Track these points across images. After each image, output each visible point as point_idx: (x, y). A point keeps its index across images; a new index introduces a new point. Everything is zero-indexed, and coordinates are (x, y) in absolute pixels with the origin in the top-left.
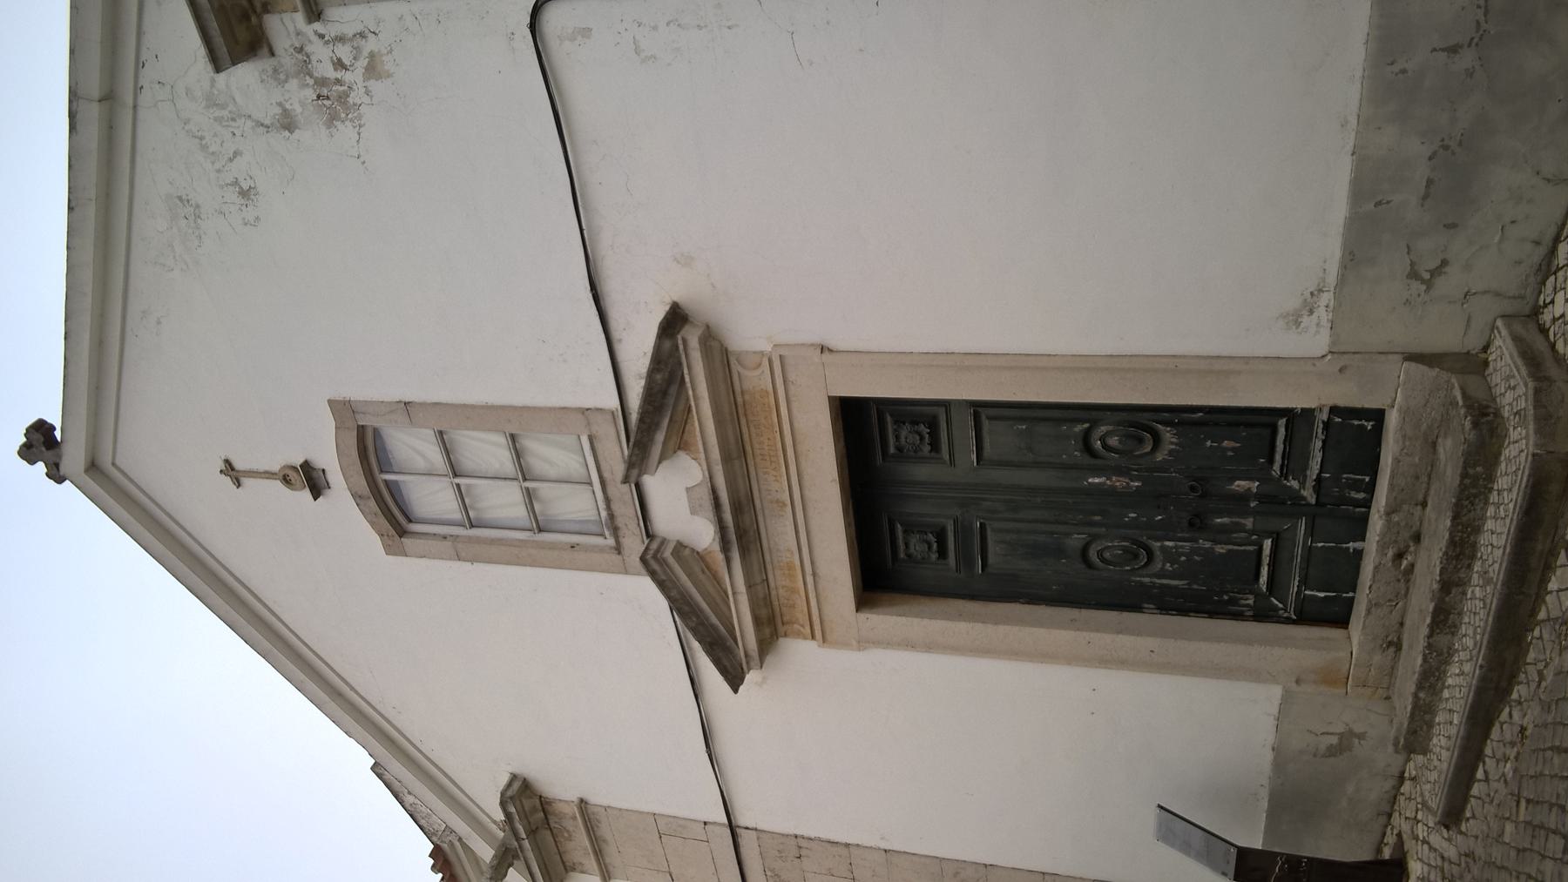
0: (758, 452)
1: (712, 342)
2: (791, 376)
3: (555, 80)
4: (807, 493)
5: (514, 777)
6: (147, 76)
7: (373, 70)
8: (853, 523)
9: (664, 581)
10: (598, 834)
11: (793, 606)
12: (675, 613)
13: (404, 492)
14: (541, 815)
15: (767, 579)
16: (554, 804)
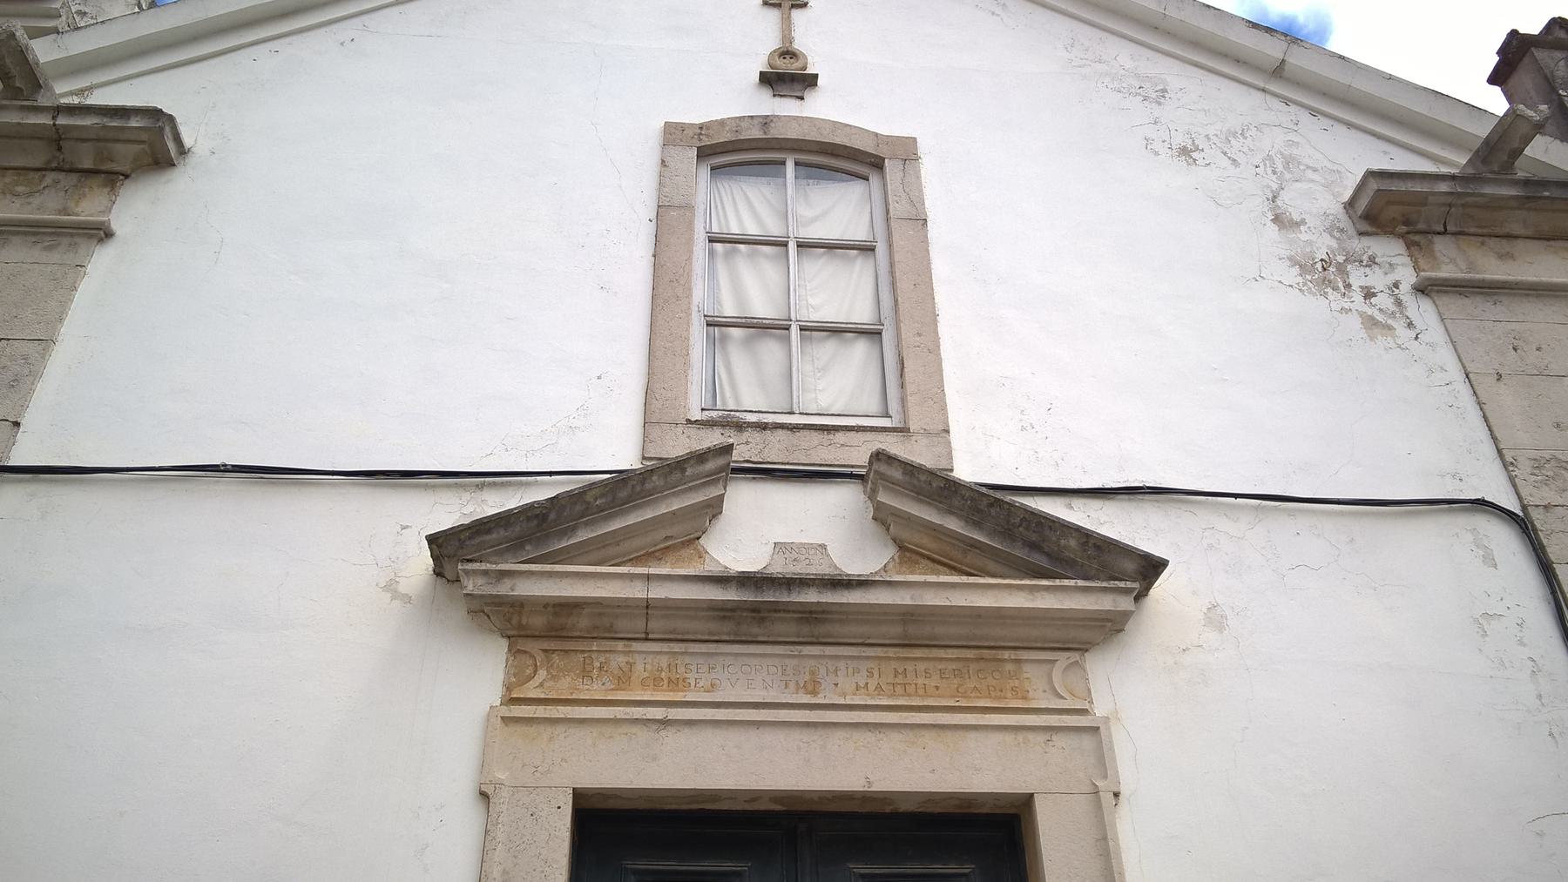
0: (910, 667)
1: (1110, 627)
2: (1060, 740)
3: (1420, 513)
4: (840, 734)
5: (183, 151)
6: (1304, 116)
7: (1370, 323)
8: (998, 811)
9: (684, 470)
10: (16, 240)
11: (585, 674)
12: (609, 476)
13: (753, 179)
14: (87, 164)
15: (647, 639)
16: (106, 190)
